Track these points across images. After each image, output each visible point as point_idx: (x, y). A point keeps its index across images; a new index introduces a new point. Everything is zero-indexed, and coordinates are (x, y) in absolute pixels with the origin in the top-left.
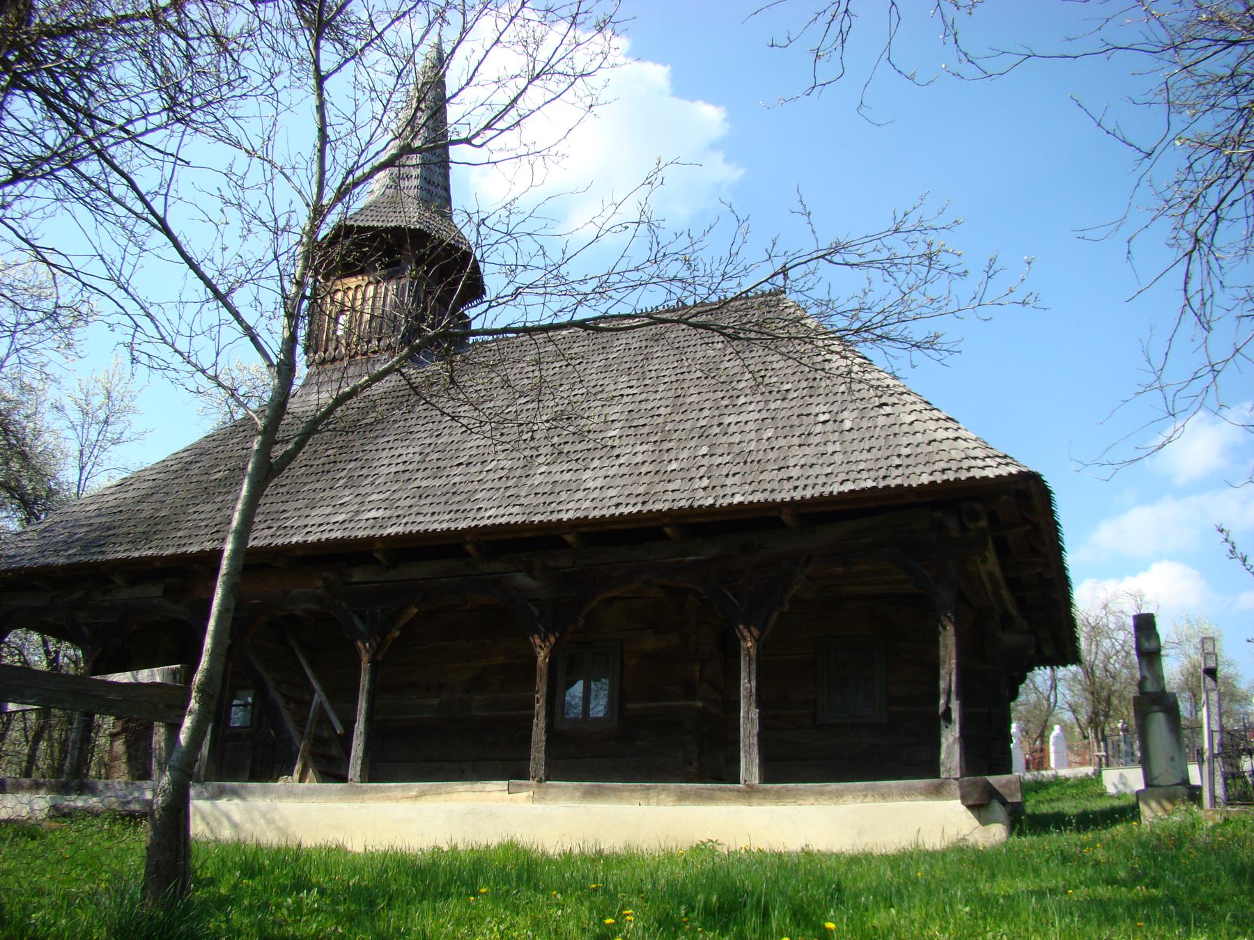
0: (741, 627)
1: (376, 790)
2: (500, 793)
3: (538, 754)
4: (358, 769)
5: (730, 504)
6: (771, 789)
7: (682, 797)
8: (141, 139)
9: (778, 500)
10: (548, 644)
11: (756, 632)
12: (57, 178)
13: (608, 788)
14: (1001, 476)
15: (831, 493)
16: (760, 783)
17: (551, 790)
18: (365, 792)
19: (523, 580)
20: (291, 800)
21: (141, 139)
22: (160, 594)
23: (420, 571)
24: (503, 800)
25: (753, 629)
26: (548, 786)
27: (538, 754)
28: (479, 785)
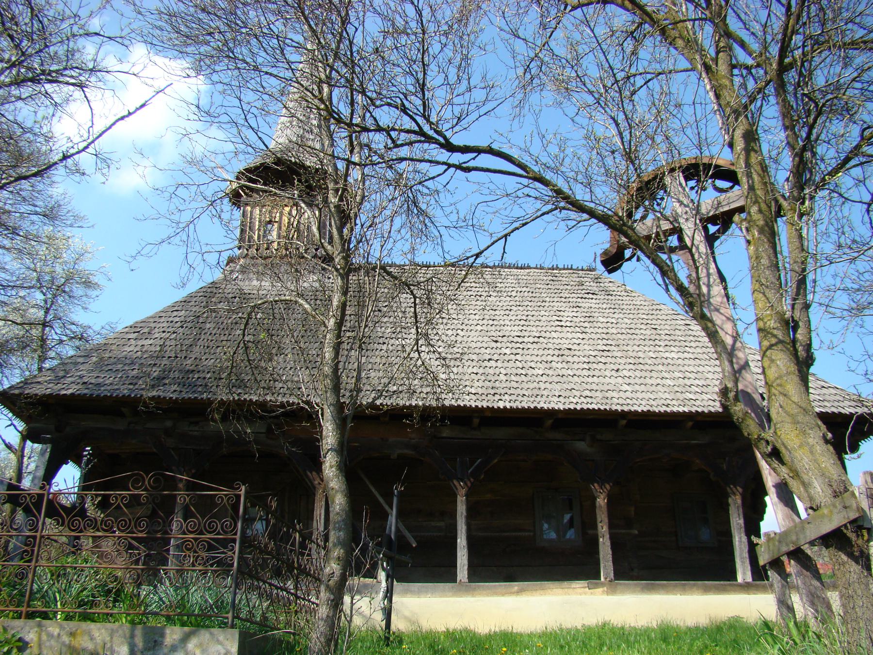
0: (732, 486)
1: (488, 588)
2: (582, 589)
3: (462, 572)
4: (466, 572)
5: (535, 407)
6: (760, 584)
7: (707, 590)
8: (416, 128)
9: (401, 404)
10: (605, 490)
11: (740, 490)
12: (83, 91)
13: (658, 585)
14: (827, 413)
15: (493, 407)
16: (753, 580)
17: (619, 587)
18: (474, 589)
19: (582, 446)
20: (408, 595)
21: (416, 128)
22: (20, 429)
23: (501, 433)
24: (585, 594)
25: (738, 488)
26: (617, 584)
27: (462, 572)
28: (566, 584)
